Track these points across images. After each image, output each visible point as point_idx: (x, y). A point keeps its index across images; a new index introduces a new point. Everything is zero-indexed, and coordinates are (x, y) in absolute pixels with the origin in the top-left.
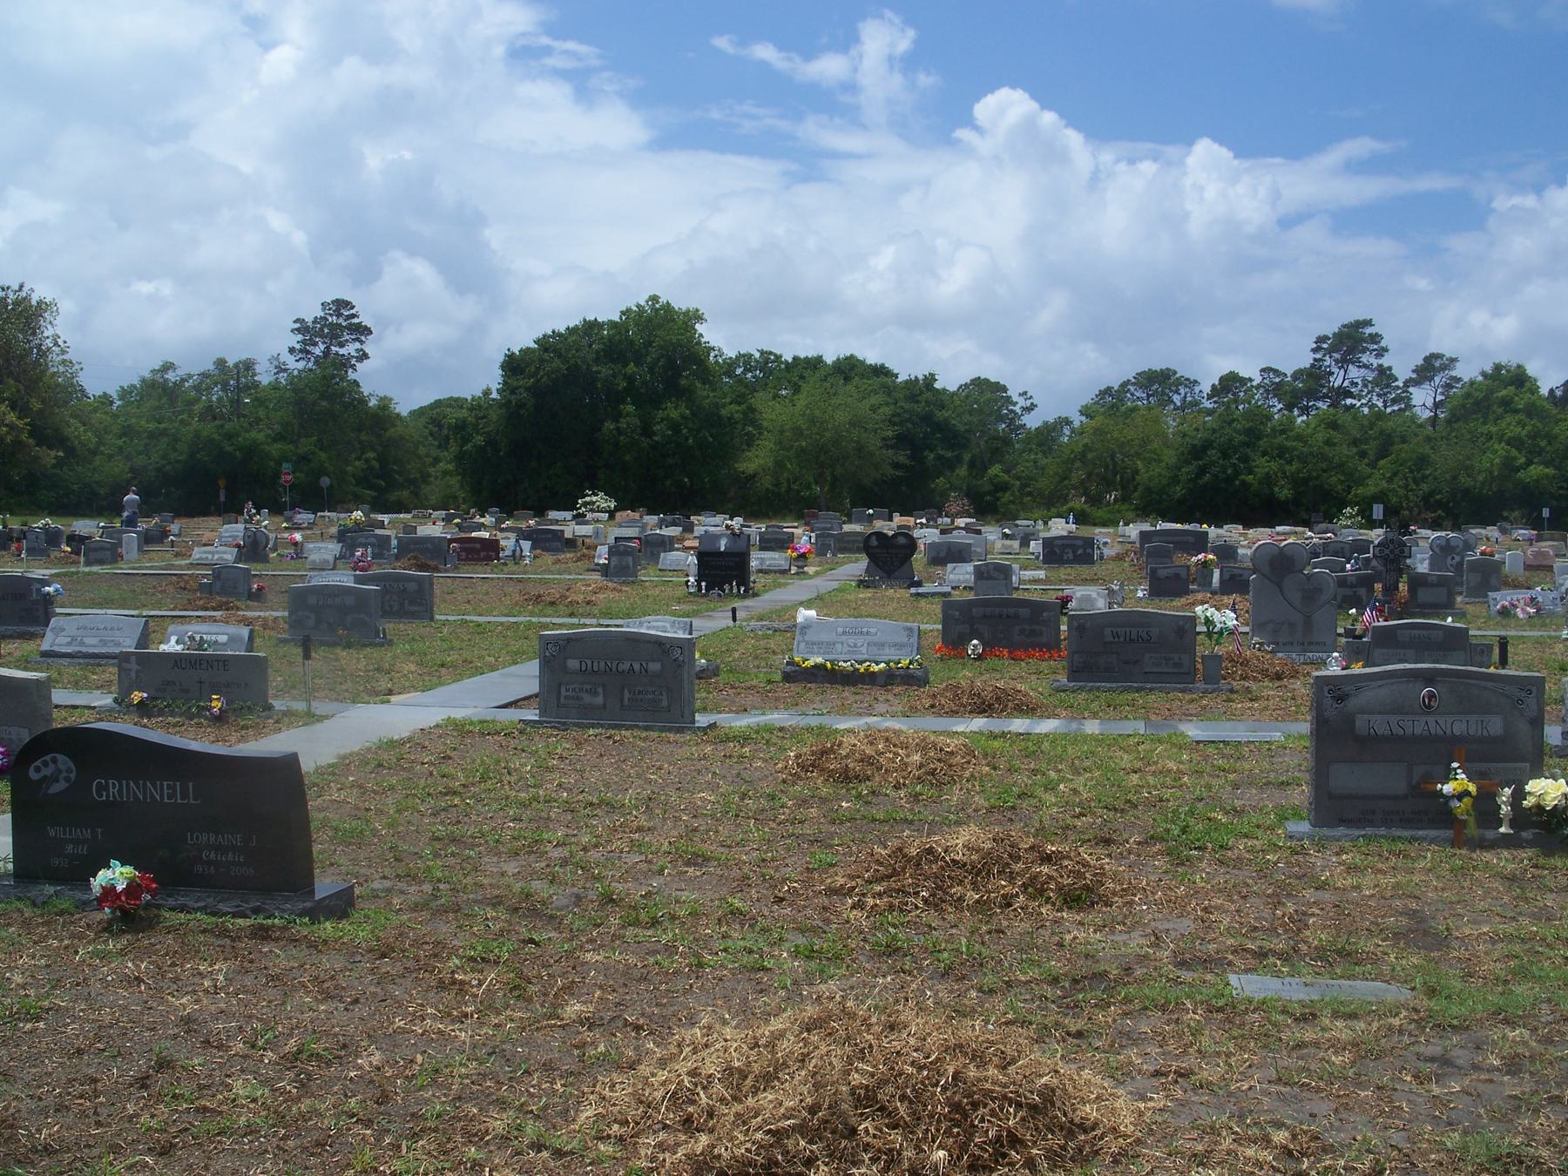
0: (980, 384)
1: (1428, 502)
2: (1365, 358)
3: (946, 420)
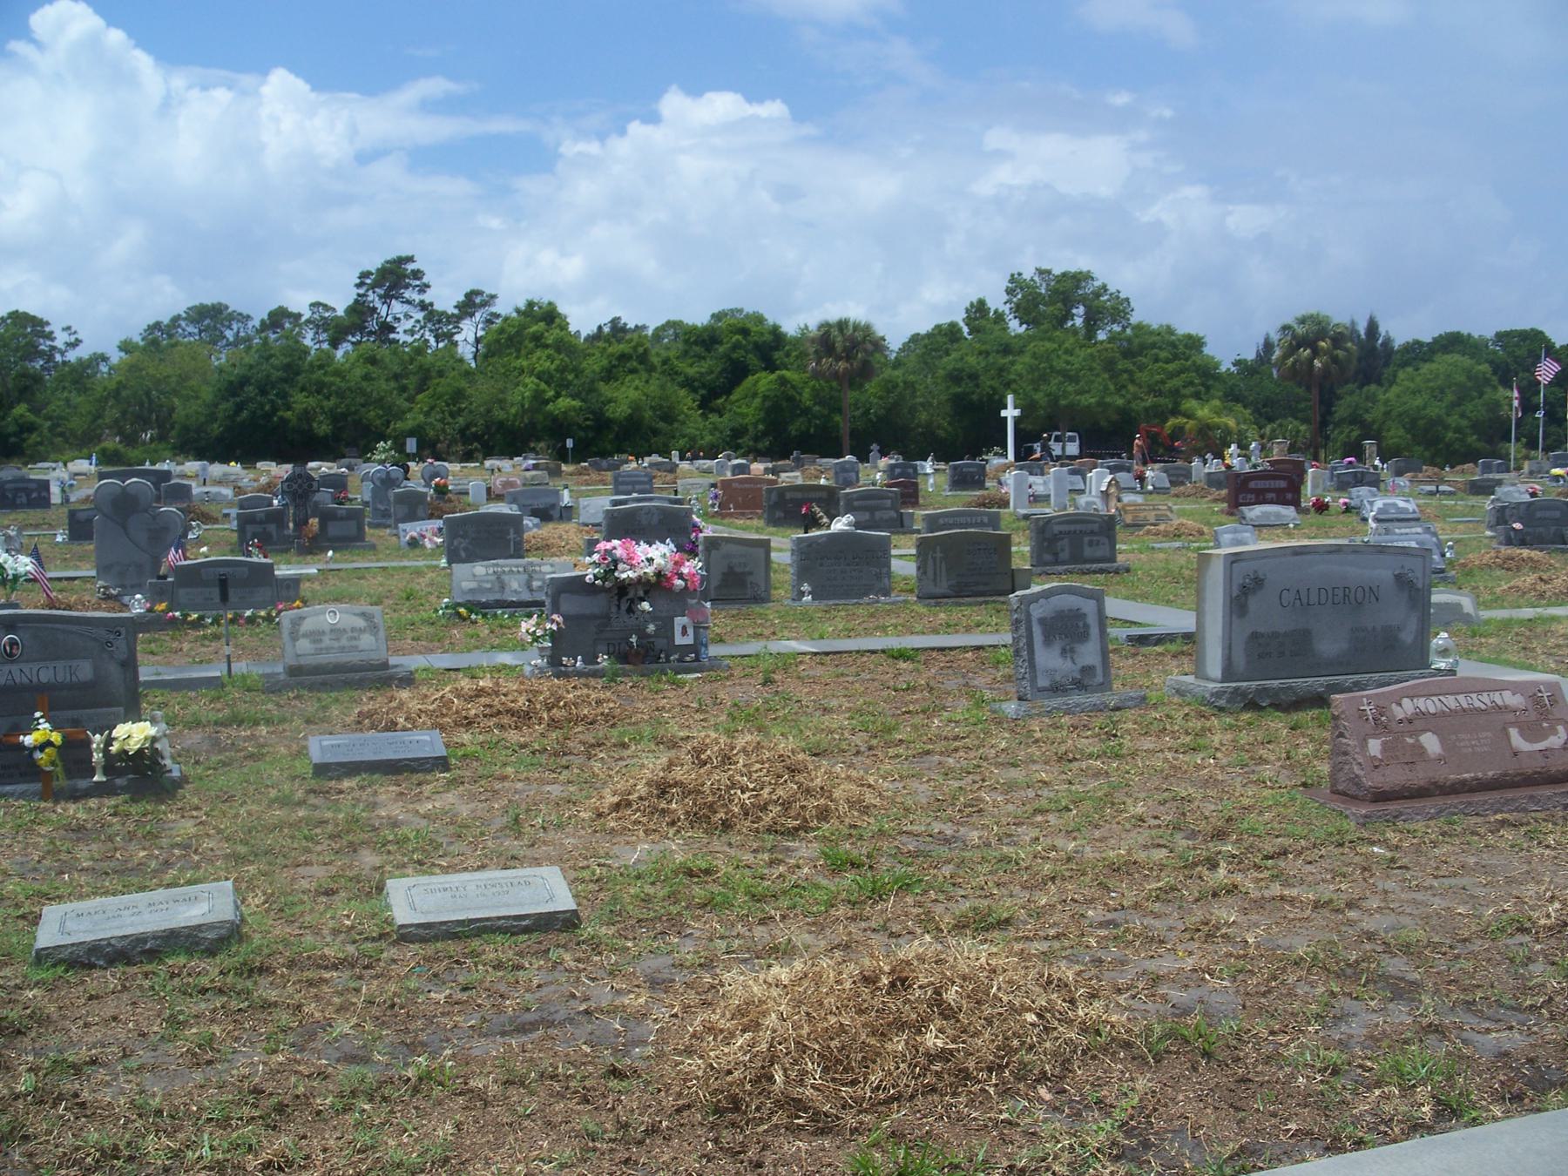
1: (465, 435)
2: (408, 294)
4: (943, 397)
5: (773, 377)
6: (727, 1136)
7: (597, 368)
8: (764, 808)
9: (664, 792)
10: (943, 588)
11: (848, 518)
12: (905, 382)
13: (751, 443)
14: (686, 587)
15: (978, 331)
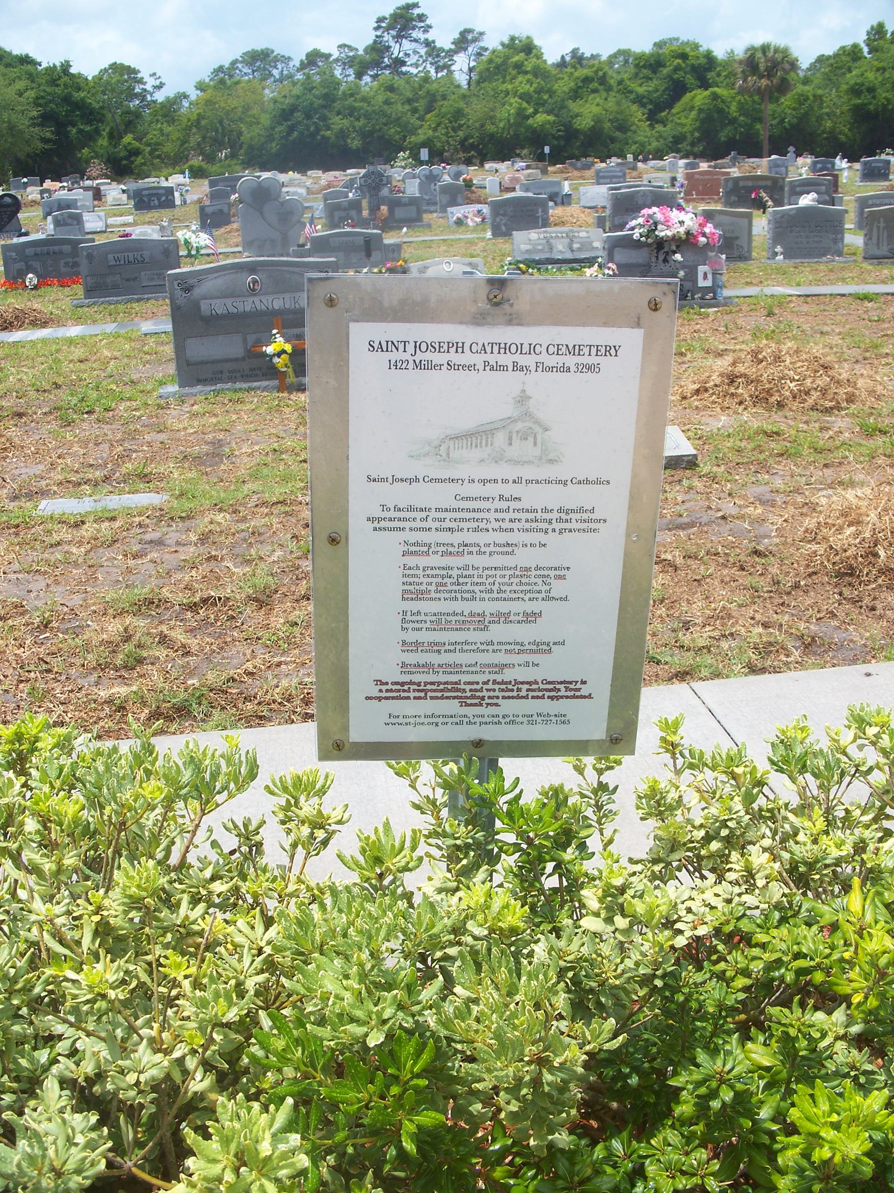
0: (116, 68)
1: (464, 145)
3: (83, 100)
4: (845, 108)
5: (707, 93)
6: (846, 592)
7: (566, 89)
8: (807, 393)
9: (732, 382)
10: (884, 250)
11: (813, 195)
12: (814, 96)
13: (689, 148)
14: (708, 243)
15: (877, 51)
